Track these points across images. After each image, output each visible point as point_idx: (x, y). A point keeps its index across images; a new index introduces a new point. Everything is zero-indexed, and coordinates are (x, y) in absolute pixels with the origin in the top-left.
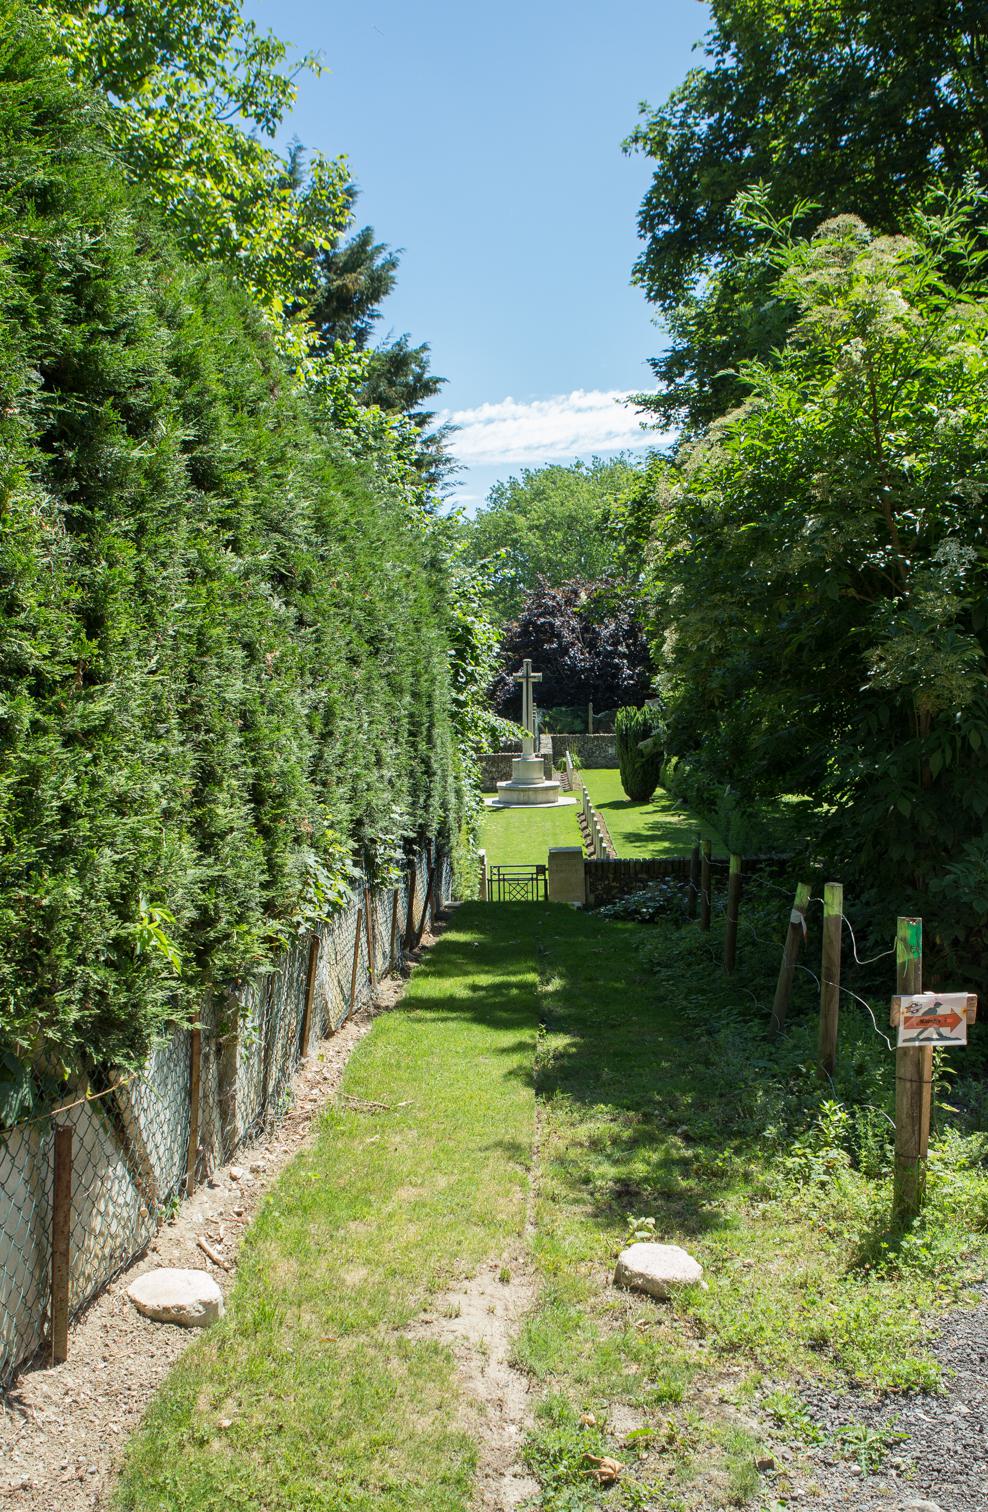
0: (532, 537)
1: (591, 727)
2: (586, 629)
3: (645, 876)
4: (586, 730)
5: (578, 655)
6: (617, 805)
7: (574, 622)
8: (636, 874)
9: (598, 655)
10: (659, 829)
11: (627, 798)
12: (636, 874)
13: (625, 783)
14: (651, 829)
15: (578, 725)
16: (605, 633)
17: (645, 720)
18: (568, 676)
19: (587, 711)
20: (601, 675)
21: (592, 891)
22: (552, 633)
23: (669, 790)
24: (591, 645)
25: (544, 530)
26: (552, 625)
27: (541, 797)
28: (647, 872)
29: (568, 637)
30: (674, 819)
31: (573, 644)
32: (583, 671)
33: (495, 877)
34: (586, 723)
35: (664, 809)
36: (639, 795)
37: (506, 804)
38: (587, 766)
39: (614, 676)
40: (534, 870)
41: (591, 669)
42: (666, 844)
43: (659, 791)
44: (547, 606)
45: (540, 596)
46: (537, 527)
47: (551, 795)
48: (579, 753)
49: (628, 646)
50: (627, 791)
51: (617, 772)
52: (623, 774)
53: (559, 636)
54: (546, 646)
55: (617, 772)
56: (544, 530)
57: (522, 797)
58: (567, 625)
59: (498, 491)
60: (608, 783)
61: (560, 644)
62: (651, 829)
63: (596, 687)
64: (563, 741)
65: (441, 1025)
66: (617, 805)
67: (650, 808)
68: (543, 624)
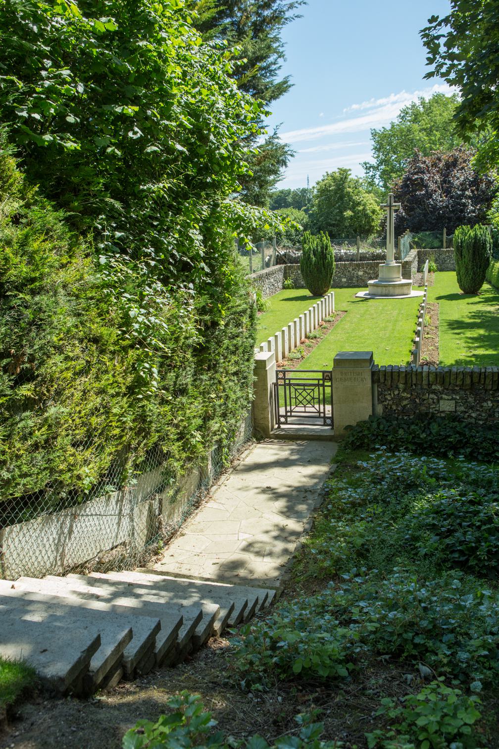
0: (423, 136)
1: (445, 244)
2: (444, 181)
3: (438, 387)
4: (442, 246)
5: (439, 199)
6: (452, 297)
7: (437, 177)
8: (429, 385)
9: (451, 197)
10: (479, 317)
11: (460, 292)
12: (429, 385)
13: (460, 281)
14: (473, 317)
15: (436, 243)
16: (457, 183)
17: (476, 235)
18: (431, 212)
19: (442, 234)
20: (453, 211)
21: (380, 402)
22: (422, 184)
23: (493, 286)
24: (447, 192)
25: (429, 132)
26: (422, 179)
27: (397, 291)
28: (442, 383)
29: (432, 186)
30: (492, 309)
31: (435, 191)
32: (440, 208)
33: (281, 382)
34: (442, 241)
35: (487, 300)
36: (470, 289)
37: (373, 296)
38: (441, 270)
39: (462, 211)
40: (320, 375)
41: (447, 207)
42: (482, 332)
43: (486, 286)
44: (420, 168)
45: (416, 160)
46: (425, 130)
47: (405, 290)
48: (436, 261)
49: (472, 191)
50: (461, 287)
51: (454, 273)
52: (458, 274)
53: (426, 186)
54: (418, 193)
55: (454, 273)
56: (429, 132)
57: (384, 291)
58: (433, 180)
59: (405, 112)
60: (449, 281)
61: (427, 191)
62: (473, 317)
63: (450, 219)
64: (425, 254)
65: (191, 573)
66: (452, 297)
67: (476, 299)
68: (416, 179)
